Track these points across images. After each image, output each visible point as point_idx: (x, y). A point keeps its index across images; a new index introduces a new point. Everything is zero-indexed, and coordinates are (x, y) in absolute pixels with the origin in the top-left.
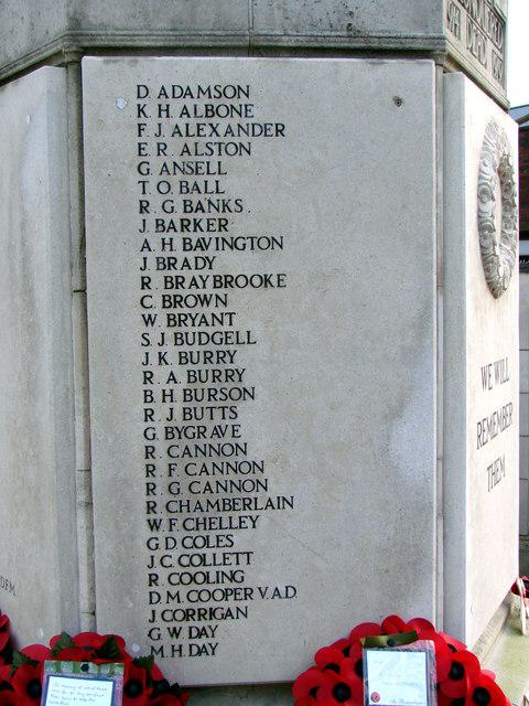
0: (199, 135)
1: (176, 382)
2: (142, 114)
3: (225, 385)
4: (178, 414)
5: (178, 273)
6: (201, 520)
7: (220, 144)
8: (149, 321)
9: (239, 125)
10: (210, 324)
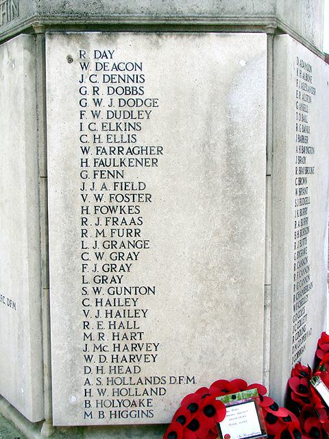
1: (106, 189)
2: (119, 129)
3: (134, 238)
4: (116, 103)
5: (119, 250)
8: (85, 151)
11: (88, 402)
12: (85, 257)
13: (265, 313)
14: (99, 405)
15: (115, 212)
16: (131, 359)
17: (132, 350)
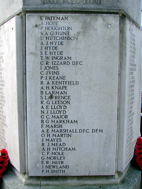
0: (55, 104)
6: (61, 37)
7: (60, 148)
9: (64, 92)
10: (63, 94)
11: (42, 121)
12: (42, 73)
13: (118, 167)
14: (48, 24)
15: (54, 168)
16: (64, 63)
17: (61, 137)
